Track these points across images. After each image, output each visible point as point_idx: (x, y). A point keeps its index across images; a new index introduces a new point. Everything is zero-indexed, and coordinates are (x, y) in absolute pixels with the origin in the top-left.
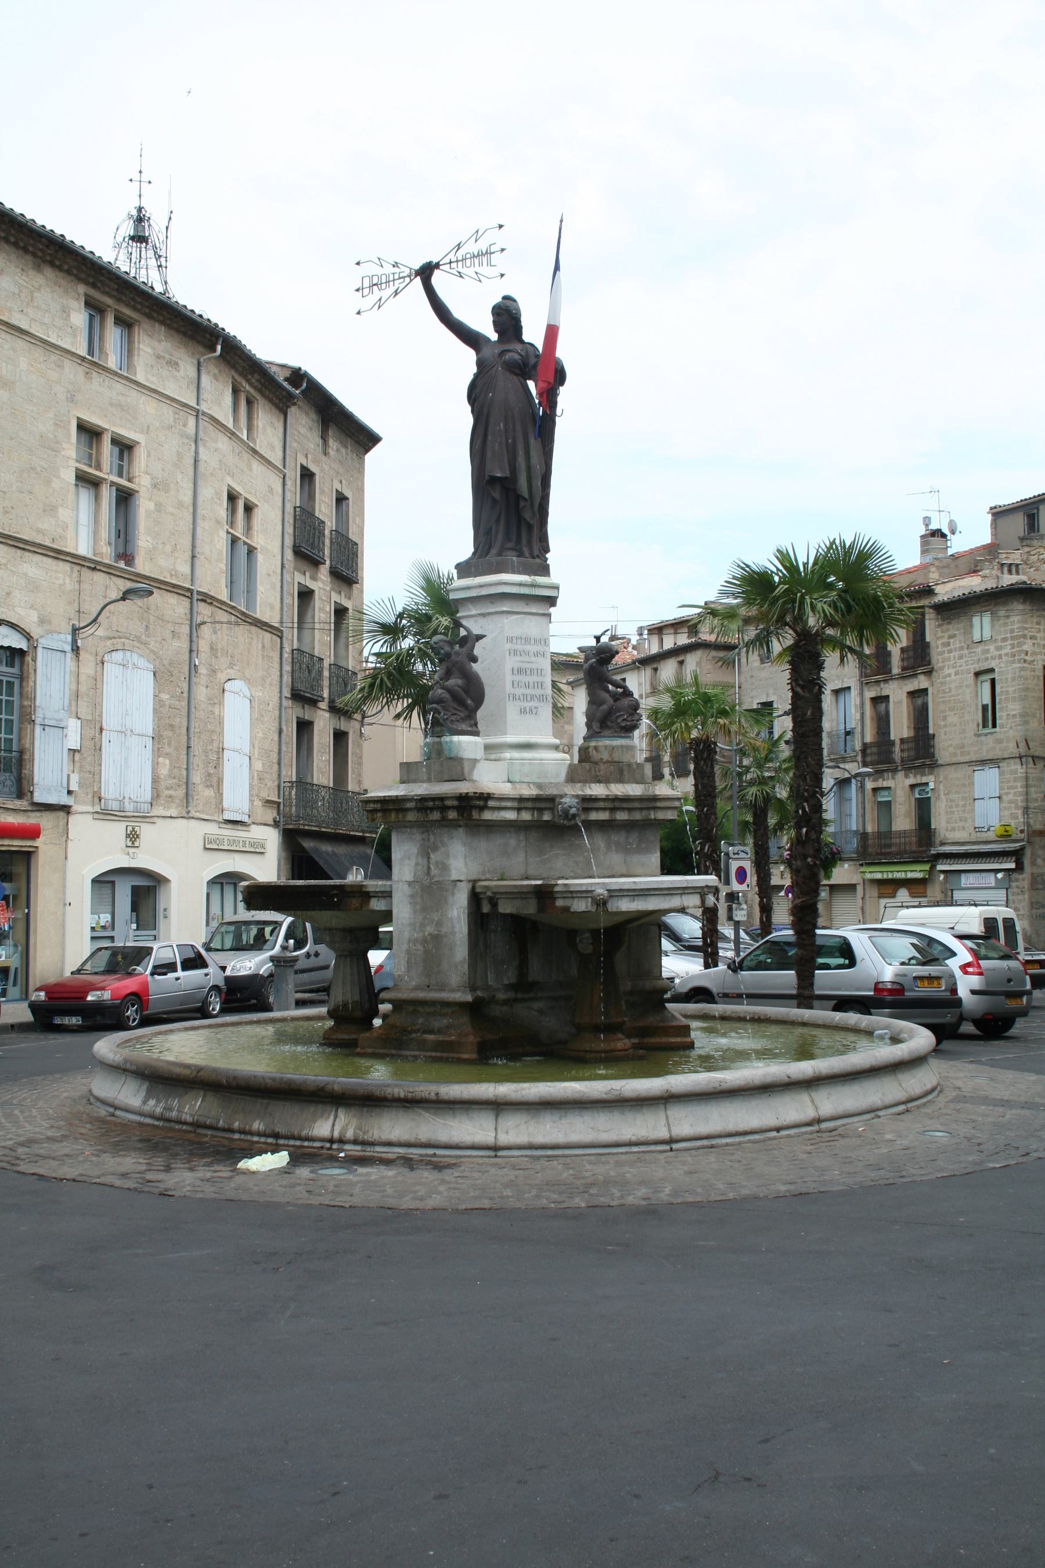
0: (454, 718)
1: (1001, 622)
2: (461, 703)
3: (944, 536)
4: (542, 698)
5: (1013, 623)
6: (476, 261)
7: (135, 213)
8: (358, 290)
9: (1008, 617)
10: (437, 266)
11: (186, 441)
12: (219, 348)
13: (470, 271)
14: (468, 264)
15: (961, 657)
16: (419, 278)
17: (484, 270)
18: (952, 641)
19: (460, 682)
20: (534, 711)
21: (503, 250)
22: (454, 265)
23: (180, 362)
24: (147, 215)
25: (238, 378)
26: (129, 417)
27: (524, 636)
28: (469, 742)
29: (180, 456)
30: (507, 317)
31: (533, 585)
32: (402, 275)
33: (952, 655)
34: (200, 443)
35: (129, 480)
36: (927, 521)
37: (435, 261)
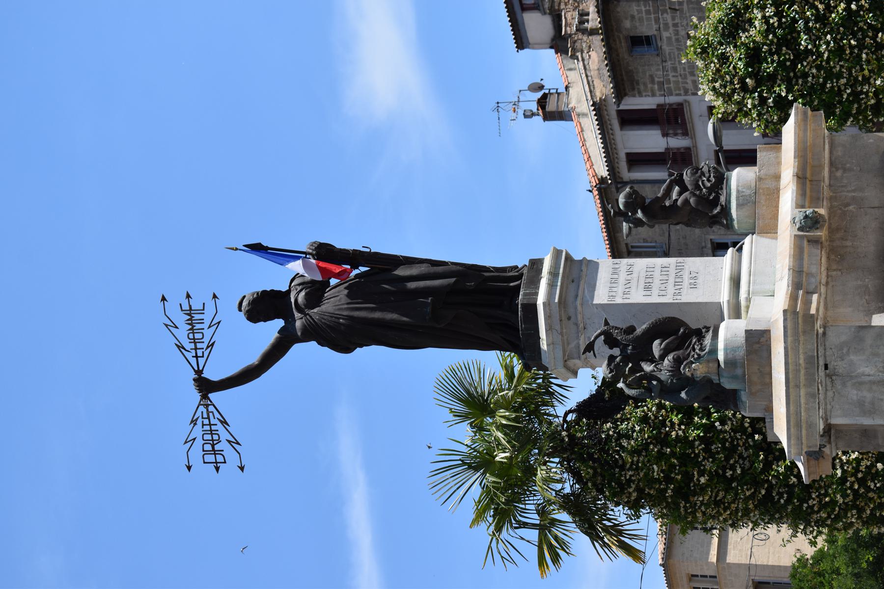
0: (697, 347)
1: (638, 24)
3: (545, 96)
4: (680, 268)
5: (640, 12)
6: (198, 326)
8: (217, 469)
9: (633, 17)
13: (208, 333)
14: (200, 336)
15: (675, 69)
16: (210, 395)
17: (207, 317)
18: (656, 79)
19: (656, 343)
20: (693, 275)
21: (188, 296)
22: (200, 353)
27: (609, 285)
30: (264, 306)
31: (553, 274)
32: (205, 415)
33: (672, 79)
36: (528, 115)
37: (193, 375)
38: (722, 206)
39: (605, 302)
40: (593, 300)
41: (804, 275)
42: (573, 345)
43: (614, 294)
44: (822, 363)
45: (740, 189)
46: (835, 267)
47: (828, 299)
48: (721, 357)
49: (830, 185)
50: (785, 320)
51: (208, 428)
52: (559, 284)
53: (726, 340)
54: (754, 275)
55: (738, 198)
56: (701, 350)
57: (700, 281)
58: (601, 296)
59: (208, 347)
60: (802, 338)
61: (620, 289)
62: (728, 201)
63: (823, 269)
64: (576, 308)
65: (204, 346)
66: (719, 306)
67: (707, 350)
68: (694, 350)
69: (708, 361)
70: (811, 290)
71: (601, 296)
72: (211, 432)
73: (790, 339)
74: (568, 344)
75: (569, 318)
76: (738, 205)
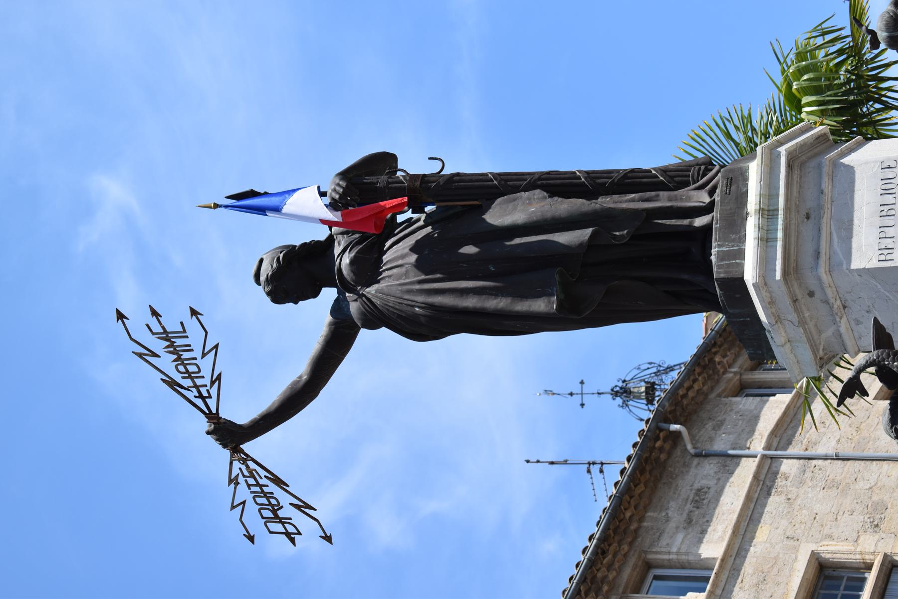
7: (619, 401)
8: (293, 541)
10: (212, 416)
11: (808, 474)
12: (675, 427)
13: (206, 365)
17: (195, 337)
21: (154, 313)
23: (697, 486)
24: (620, 384)
26: (775, 570)
27: (879, 222)
29: (831, 485)
30: (295, 274)
31: (768, 213)
35: (869, 567)
37: (204, 424)
39: (874, 264)
42: (829, 333)
43: (889, 243)
51: (257, 489)
52: (780, 235)
58: (864, 254)
59: (212, 383)
64: (819, 279)
65: (207, 381)
71: (864, 254)
72: (265, 495)
74: (820, 332)
75: (811, 294)
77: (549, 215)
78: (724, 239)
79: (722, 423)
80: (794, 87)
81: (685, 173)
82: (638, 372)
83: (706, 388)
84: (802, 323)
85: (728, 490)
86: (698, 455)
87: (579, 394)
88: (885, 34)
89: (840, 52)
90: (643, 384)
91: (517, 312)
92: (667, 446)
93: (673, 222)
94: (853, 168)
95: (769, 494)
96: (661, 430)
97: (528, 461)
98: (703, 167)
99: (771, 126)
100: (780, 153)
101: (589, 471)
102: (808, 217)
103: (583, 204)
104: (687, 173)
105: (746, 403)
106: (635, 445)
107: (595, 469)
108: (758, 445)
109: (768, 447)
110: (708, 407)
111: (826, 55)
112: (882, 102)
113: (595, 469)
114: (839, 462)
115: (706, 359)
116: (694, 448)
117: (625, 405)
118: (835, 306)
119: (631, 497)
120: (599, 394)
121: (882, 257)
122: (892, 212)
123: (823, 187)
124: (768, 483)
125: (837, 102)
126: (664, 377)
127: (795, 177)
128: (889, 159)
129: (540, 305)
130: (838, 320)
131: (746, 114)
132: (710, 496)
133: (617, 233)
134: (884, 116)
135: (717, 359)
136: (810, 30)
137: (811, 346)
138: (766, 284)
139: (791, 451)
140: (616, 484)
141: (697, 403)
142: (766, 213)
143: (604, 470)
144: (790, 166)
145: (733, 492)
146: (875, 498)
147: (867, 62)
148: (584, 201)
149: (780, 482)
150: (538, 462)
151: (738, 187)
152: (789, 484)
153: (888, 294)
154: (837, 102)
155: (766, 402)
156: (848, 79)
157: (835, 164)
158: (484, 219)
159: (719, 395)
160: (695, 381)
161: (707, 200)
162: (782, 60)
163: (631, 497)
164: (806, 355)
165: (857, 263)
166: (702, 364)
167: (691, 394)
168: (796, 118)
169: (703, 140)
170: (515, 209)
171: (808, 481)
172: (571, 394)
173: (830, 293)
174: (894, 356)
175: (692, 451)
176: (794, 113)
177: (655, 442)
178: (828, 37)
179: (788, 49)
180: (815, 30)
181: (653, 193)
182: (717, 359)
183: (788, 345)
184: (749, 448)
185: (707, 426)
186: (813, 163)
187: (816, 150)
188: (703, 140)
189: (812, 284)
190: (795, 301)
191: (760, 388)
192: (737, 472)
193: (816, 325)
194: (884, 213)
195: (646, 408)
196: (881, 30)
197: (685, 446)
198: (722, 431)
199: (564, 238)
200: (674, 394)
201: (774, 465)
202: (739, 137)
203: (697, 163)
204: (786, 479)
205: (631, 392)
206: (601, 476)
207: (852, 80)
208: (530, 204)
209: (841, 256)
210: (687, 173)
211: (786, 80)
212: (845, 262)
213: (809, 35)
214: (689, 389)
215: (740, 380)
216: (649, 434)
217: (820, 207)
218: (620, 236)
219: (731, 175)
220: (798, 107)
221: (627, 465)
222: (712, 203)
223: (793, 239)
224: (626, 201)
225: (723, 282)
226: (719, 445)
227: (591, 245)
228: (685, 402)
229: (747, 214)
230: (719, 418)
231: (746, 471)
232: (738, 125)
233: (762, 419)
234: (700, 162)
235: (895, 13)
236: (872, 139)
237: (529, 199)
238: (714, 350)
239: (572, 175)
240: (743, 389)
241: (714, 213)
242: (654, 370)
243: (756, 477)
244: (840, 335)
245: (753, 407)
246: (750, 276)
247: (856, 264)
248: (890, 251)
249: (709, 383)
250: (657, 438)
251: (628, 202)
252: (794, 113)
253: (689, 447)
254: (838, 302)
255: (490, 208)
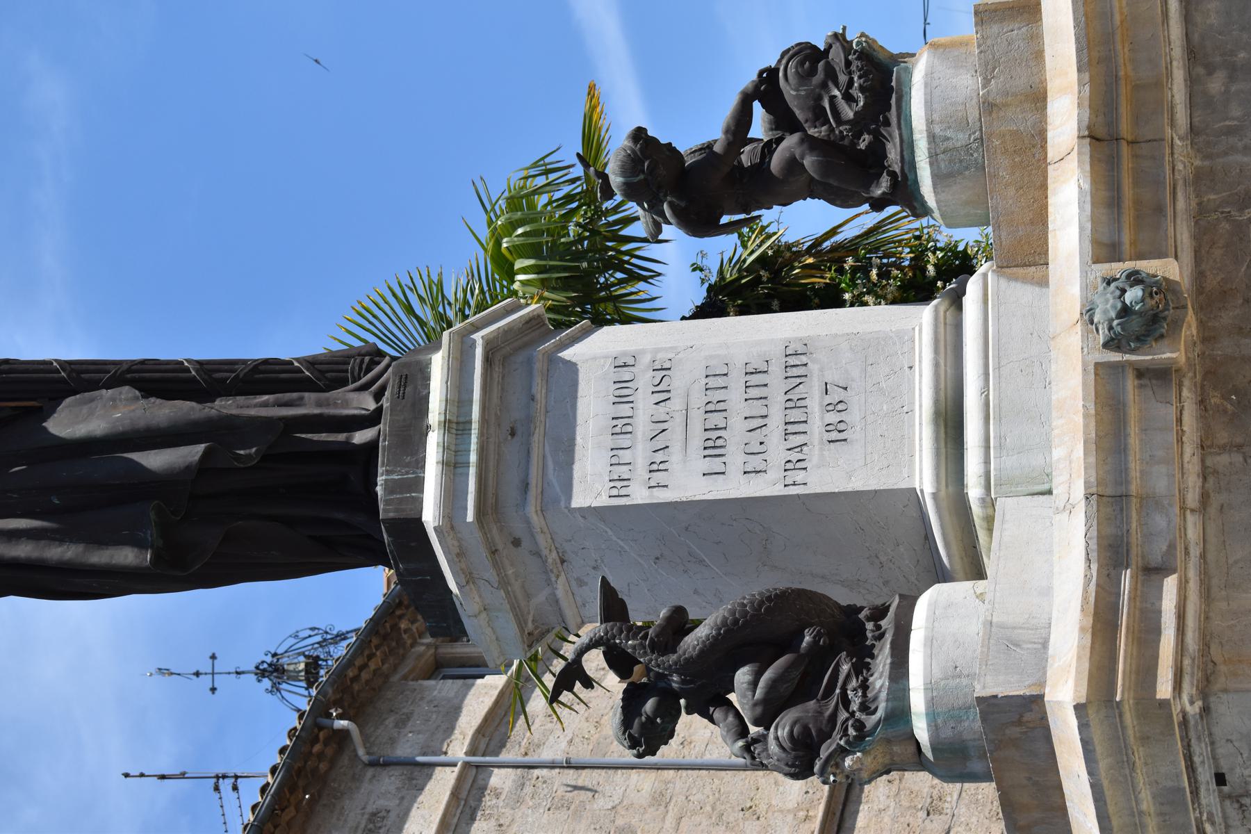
2: (821, 658)
7: (267, 683)
11: (528, 789)
19: (742, 676)
23: (371, 808)
24: (269, 659)
25: (404, 670)
27: (609, 441)
28: (930, 657)
31: (456, 426)
34: (532, 758)
38: (893, 174)
39: (603, 501)
40: (569, 497)
41: (1134, 503)
42: (541, 597)
43: (623, 471)
44: (1205, 775)
45: (937, 129)
46: (1223, 437)
47: (1211, 557)
48: (921, 731)
49: (1193, 130)
50: (1083, 727)
52: (473, 458)
53: (929, 687)
54: (999, 420)
55: (933, 158)
56: (866, 708)
57: (853, 416)
58: (590, 487)
60: (1139, 755)
61: (640, 455)
62: (909, 163)
63: (1188, 450)
64: (528, 522)
66: (912, 496)
67: (880, 713)
68: (846, 702)
69: (888, 741)
70: (1156, 558)
71: (590, 487)
73: (1103, 765)
74: (528, 596)
75: (517, 543)
76: (937, 178)
77: (142, 424)
78: (394, 463)
79: (408, 717)
80: (505, 245)
81: (341, 367)
82: (295, 641)
83: (386, 666)
84: (504, 583)
85: (415, 813)
86: (374, 764)
87: (209, 674)
88: (620, 180)
89: (569, 198)
90: (302, 658)
91: (93, 565)
92: (329, 751)
93: (323, 437)
94: (575, 365)
95: (473, 819)
96: (321, 728)
97: (127, 775)
98: (367, 359)
99: (472, 294)
100: (474, 341)
101: (217, 789)
102: (513, 434)
103: (193, 408)
104: (344, 367)
105: (443, 688)
106: (282, 751)
107: (226, 785)
108: (458, 748)
109: (472, 751)
110: (389, 694)
111: (550, 203)
112: (624, 271)
113: (226, 785)
114: (572, 771)
115: (388, 625)
116: (368, 753)
117: (275, 689)
118: (550, 560)
119: (276, 827)
120: (238, 673)
121: (615, 492)
122: (629, 429)
123: (534, 391)
124: (473, 804)
125: (565, 269)
126: (332, 648)
127: (495, 376)
128: (625, 354)
129: (126, 556)
130: (553, 579)
131: (435, 279)
132: (389, 822)
133: (242, 452)
134: (630, 289)
135: (403, 626)
136: (528, 165)
137: (516, 616)
138: (452, 528)
139: (505, 756)
140: (254, 808)
141: (374, 689)
142: (454, 426)
143: (240, 786)
144: (488, 361)
145: (423, 817)
146: (620, 822)
147: (607, 213)
148: (194, 404)
149: (488, 801)
150: (142, 775)
151: (416, 388)
152: (501, 804)
153: (621, 543)
154: (565, 269)
155: (470, 687)
156: (579, 235)
157: (552, 359)
158: (45, 428)
159: (405, 678)
160: (370, 657)
161: (372, 406)
162: (489, 208)
163: (276, 827)
164: (509, 628)
165: (579, 500)
166: (382, 632)
167: (365, 676)
168: (508, 289)
169: (375, 316)
170: (91, 413)
171: (527, 798)
172: (197, 674)
173: (543, 541)
174: (629, 632)
175: (365, 758)
176: (505, 283)
177: (312, 747)
178: (552, 177)
179: (498, 190)
180: (535, 165)
181: (295, 395)
182: (403, 625)
183: (484, 615)
184: (446, 753)
185: (387, 722)
186: (520, 357)
187: (526, 339)
188: (375, 316)
189: (518, 529)
190: (494, 552)
191: (463, 666)
192: (428, 787)
193: (523, 587)
194: (617, 430)
195: (306, 693)
196: (614, 173)
197: (355, 750)
198: (408, 729)
199: (155, 460)
200: (339, 675)
201: (481, 777)
202: (425, 313)
203: (360, 354)
204: (497, 796)
205: (284, 670)
206: (235, 795)
207: (586, 238)
208: (115, 407)
209: (558, 489)
210: (344, 367)
211: (493, 234)
212: (563, 498)
213: (525, 173)
214: (361, 668)
215: (435, 655)
216: (303, 734)
217: (529, 420)
218: (246, 456)
219: (405, 372)
220: (510, 274)
221: (270, 780)
222: (379, 411)
223: (492, 464)
224: (255, 406)
225: (393, 525)
226: (403, 750)
227: (203, 467)
228: (356, 687)
229: (428, 427)
230: (405, 710)
231: (441, 785)
232: (424, 295)
233: (465, 711)
234: (363, 351)
235: (633, 151)
236: (611, 322)
237: (114, 400)
238: (398, 612)
239: (178, 366)
240: (438, 668)
241: (381, 426)
242: (318, 638)
243: (455, 794)
244: (557, 601)
245: (452, 694)
246: (430, 515)
247: (578, 501)
248: (625, 483)
249: (391, 660)
250: (315, 740)
251: (259, 407)
252: (505, 283)
253: (361, 752)
254: (554, 554)
255: (54, 411)
